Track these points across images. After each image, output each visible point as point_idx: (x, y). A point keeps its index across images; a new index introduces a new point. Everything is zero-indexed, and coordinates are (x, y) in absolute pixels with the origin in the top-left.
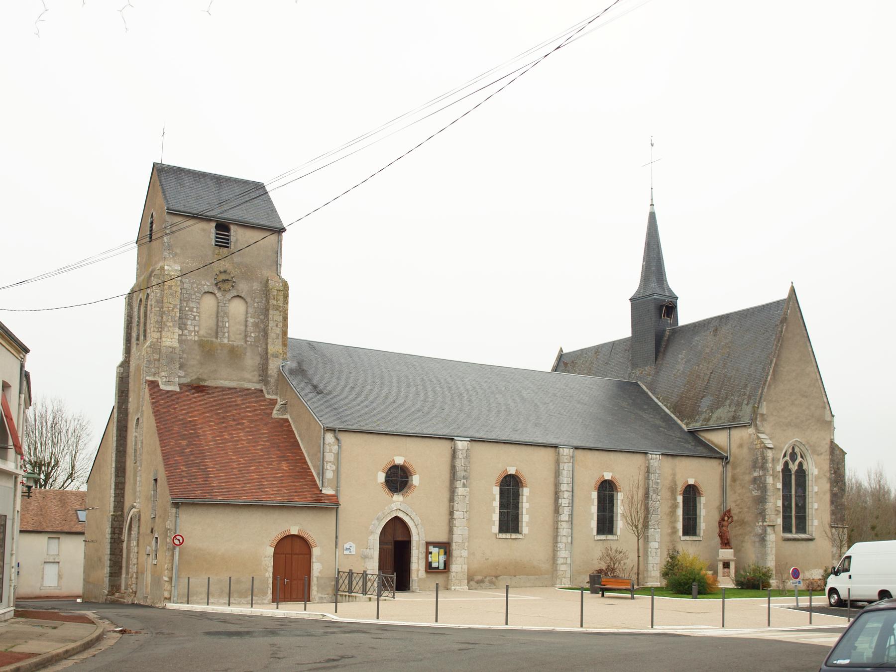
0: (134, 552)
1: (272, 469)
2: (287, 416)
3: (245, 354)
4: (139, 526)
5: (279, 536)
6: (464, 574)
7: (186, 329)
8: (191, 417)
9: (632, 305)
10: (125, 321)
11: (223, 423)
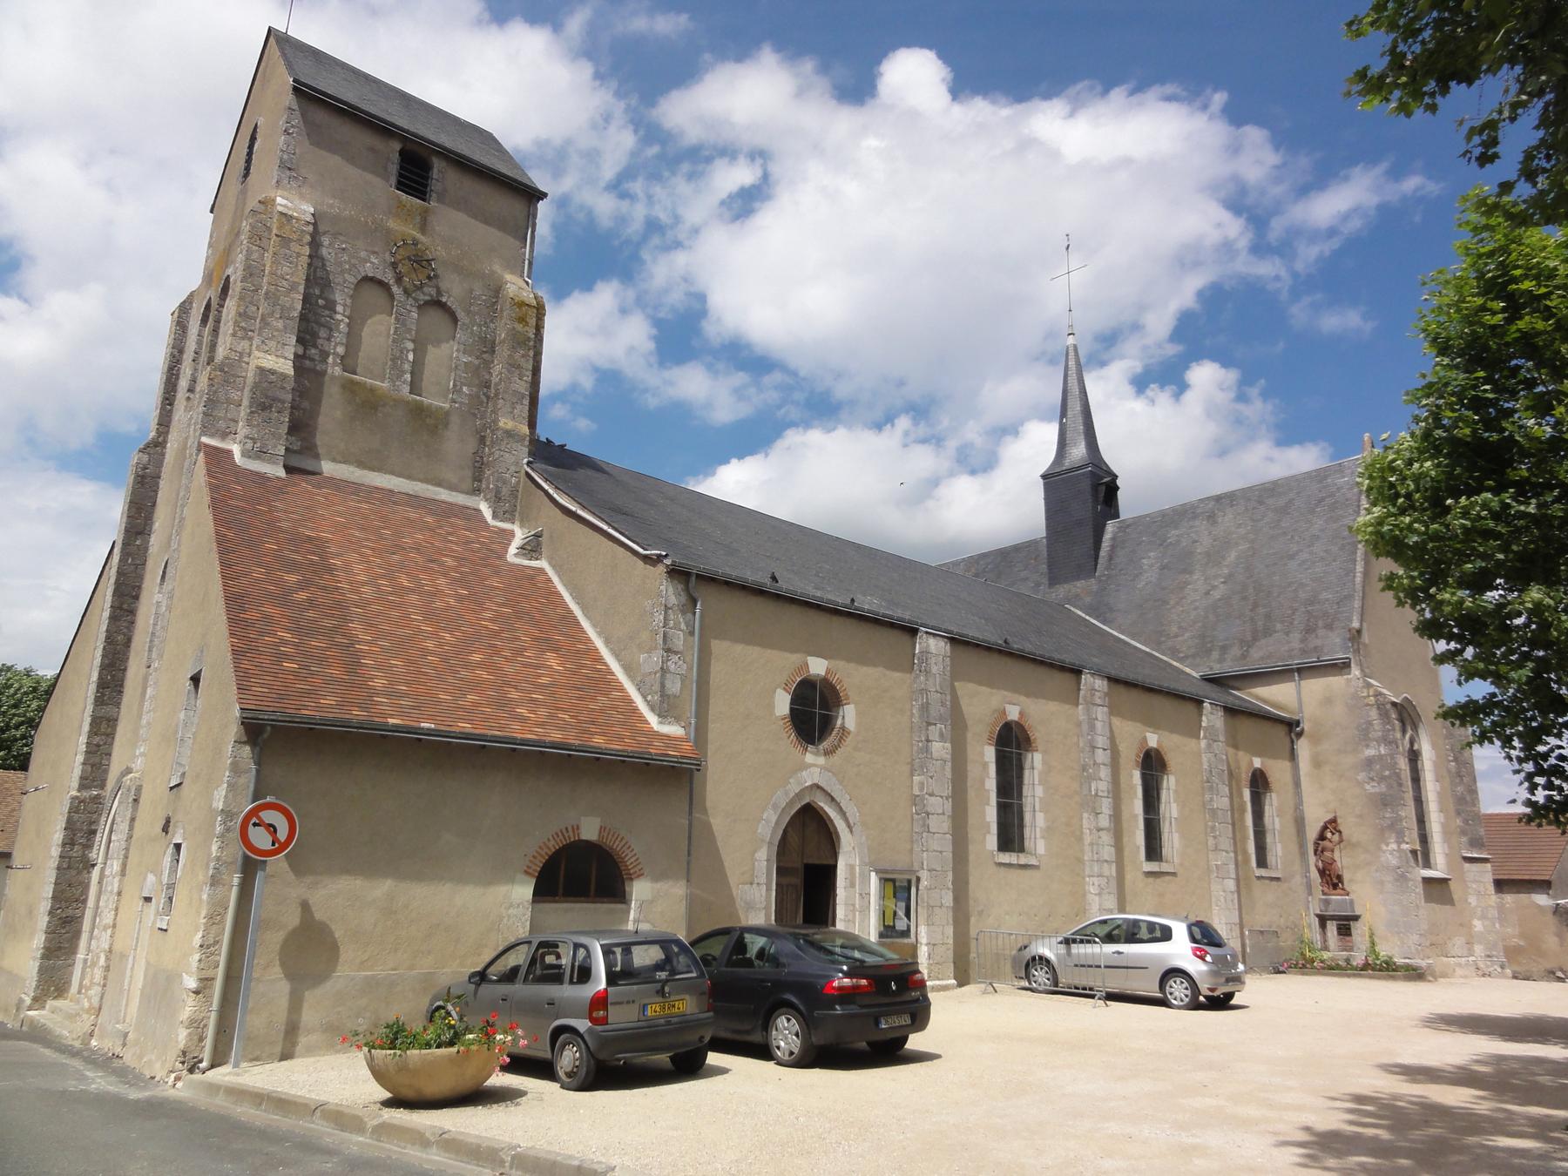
0: (111, 892)
1: (525, 665)
2: (542, 564)
3: (446, 425)
4: (133, 820)
5: (543, 853)
6: (948, 949)
7: (315, 346)
8: (312, 529)
9: (1045, 484)
10: (166, 358)
11: (394, 554)
